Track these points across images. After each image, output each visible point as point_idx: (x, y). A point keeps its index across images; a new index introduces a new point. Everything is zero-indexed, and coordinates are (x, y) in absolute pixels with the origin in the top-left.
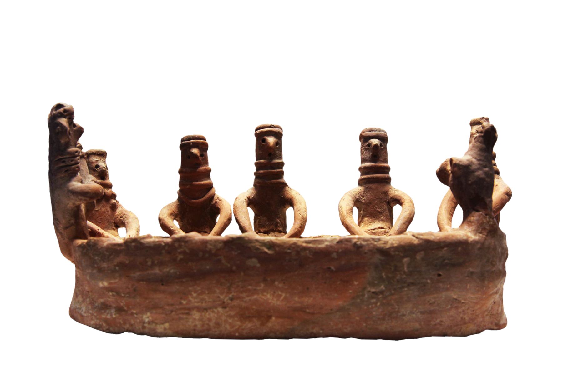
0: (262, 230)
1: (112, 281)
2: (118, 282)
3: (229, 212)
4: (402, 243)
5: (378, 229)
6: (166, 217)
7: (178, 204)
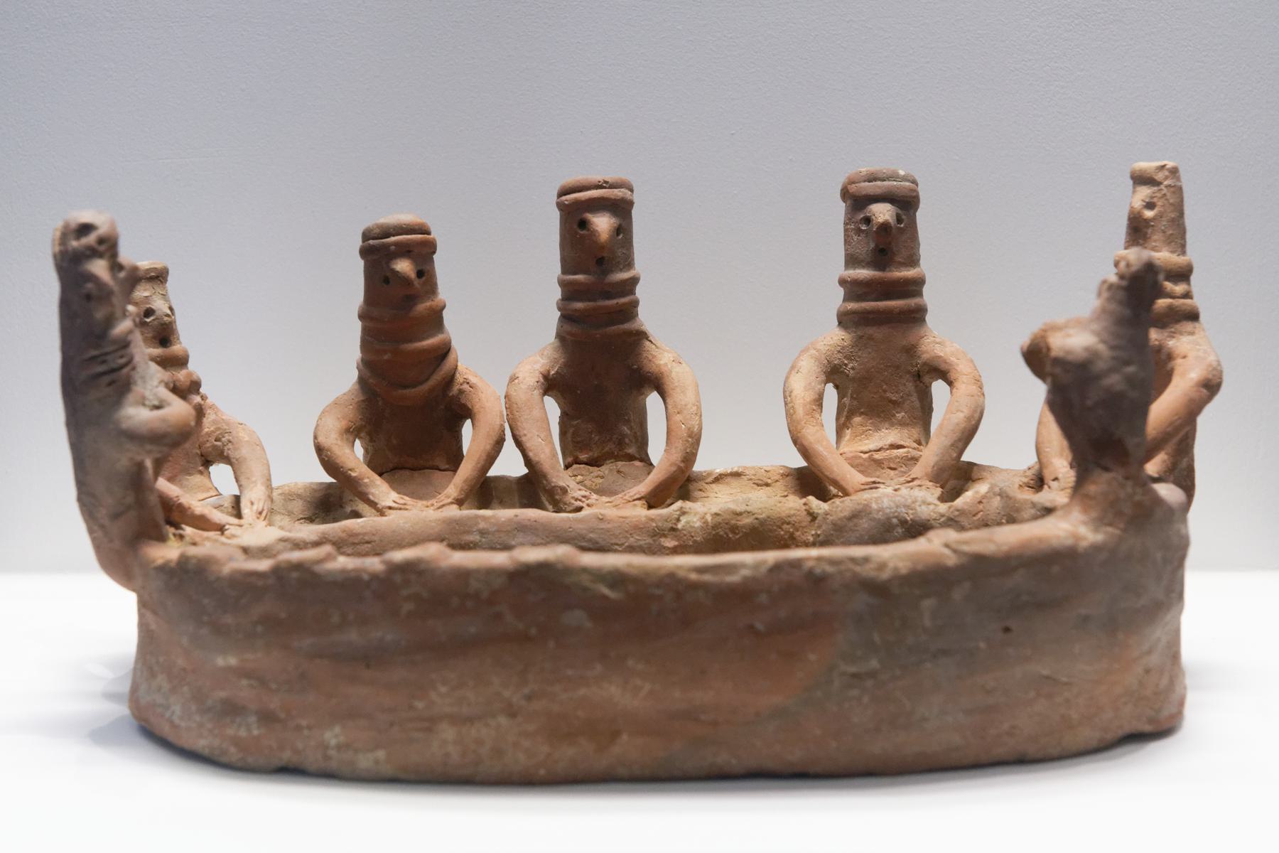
0: (583, 457)
1: (249, 656)
2: (257, 658)
3: (498, 422)
4: (920, 567)
5: (887, 449)
6: (335, 442)
7: (363, 401)
